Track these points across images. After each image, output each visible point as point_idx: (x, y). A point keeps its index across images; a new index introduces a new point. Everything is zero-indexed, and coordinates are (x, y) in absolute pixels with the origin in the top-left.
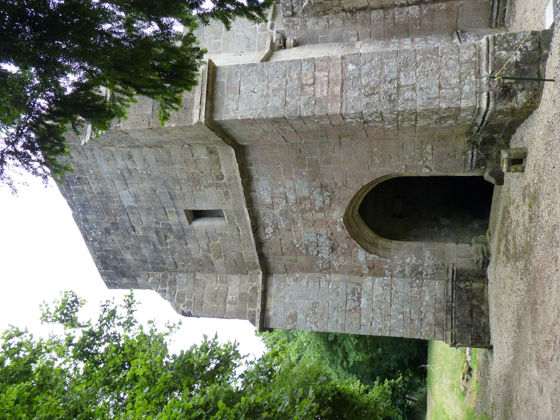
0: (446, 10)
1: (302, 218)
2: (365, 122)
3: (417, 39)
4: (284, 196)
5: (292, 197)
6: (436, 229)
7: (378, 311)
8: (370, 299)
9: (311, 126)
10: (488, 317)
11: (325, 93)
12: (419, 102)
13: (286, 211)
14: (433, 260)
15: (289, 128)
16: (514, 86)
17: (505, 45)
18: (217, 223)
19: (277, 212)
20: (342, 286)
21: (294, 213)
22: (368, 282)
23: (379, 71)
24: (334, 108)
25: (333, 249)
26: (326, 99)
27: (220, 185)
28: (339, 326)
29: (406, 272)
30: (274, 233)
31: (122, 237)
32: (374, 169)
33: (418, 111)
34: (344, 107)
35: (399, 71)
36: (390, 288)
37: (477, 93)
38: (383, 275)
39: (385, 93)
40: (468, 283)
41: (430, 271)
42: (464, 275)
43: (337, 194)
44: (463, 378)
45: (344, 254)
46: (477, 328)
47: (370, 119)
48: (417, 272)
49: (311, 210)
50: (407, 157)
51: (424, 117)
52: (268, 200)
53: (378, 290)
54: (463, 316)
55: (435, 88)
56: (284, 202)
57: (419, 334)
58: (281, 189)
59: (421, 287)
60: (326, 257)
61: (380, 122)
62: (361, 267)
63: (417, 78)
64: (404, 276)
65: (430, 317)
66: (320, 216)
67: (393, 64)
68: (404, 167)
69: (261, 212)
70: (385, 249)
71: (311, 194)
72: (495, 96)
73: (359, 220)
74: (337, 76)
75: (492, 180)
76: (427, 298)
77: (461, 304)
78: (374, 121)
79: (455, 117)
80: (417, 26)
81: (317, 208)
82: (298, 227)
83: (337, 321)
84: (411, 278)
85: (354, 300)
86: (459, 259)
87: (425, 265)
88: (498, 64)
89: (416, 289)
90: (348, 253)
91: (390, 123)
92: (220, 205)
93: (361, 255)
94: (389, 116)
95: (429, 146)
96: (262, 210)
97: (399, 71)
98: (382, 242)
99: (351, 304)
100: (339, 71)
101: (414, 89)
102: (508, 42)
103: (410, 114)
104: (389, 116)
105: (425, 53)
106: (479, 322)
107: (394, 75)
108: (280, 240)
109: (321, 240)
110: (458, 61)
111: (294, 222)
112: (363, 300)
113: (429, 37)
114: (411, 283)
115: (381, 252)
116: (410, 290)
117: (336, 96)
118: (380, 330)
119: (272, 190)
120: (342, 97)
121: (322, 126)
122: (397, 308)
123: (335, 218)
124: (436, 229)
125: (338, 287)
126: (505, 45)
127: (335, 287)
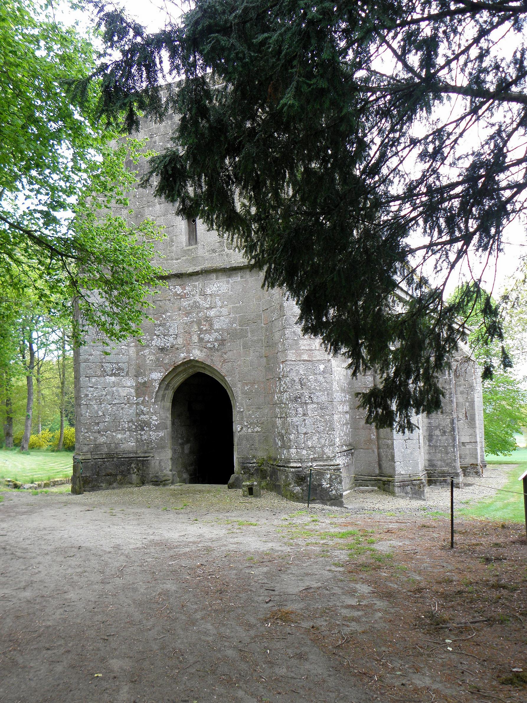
0: (370, 439)
1: (193, 322)
2: (280, 378)
3: (348, 416)
4: (213, 305)
5: (212, 313)
6: (180, 441)
7: (104, 393)
8: (114, 384)
9: (277, 335)
10: (107, 489)
11: (302, 348)
12: (295, 419)
13: (198, 307)
14: (156, 439)
15: (275, 316)
16: (305, 484)
17: (334, 477)
18: (183, 238)
19: (197, 298)
20: (125, 358)
21: (197, 314)
22: (130, 382)
23: (318, 388)
24: (291, 355)
25: (162, 350)
26: (298, 349)
27: (222, 246)
28: (87, 356)
29: (142, 416)
30: (176, 294)
31: (163, 133)
32: (239, 386)
33: (288, 419)
34: (292, 363)
35: (318, 403)
36: (126, 402)
37: (301, 459)
38: (138, 396)
39: (302, 394)
40: (135, 470)
41: (145, 437)
42: (143, 466)
43: (217, 354)
44: (9, 481)
45: (158, 359)
46: (96, 480)
47: (282, 383)
48: (142, 426)
49: (201, 330)
50: (250, 412)
51: (284, 423)
52: (209, 292)
53: (123, 392)
54: (106, 468)
55: (304, 431)
56: (208, 306)
57: (86, 431)
58: (219, 303)
59: (129, 430)
60: (154, 343)
61: (280, 390)
62: (145, 375)
63: (313, 417)
64: (137, 414)
65: (102, 440)
66: (195, 338)
67: (324, 398)
68: (242, 410)
69: (197, 283)
70: (164, 396)
71: (217, 331)
72: (299, 472)
73: (191, 372)
74: (316, 356)
75: (231, 481)
76: (119, 436)
77: (117, 466)
78: (281, 385)
79: (284, 446)
80: (359, 415)
81: (202, 336)
82: (182, 318)
83: (91, 355)
84: (137, 422)
85: (113, 370)
86: (158, 462)
87: (151, 433)
88: (321, 474)
89: (126, 426)
90: (158, 363)
91: (278, 398)
92: (203, 243)
93: (157, 376)
94: (285, 397)
95: (259, 430)
96: (198, 283)
97: (318, 403)
98: (170, 394)
99: (108, 367)
100: (318, 358)
101: (304, 415)
102: (336, 478)
103: (286, 413)
104: (285, 397)
105: (331, 422)
106: (102, 482)
107: (315, 400)
108: (169, 300)
109: (171, 339)
110: (324, 446)
111: (188, 314)
112: (113, 379)
113: (349, 426)
114: (132, 421)
115: (161, 393)
116: (125, 420)
117: (300, 356)
118: (87, 395)
119: (219, 295)
120: (300, 361)
121: (276, 344)
122: (108, 410)
123: (193, 351)
124: (180, 441)
125: (123, 354)
126: (334, 477)
127: (124, 352)
